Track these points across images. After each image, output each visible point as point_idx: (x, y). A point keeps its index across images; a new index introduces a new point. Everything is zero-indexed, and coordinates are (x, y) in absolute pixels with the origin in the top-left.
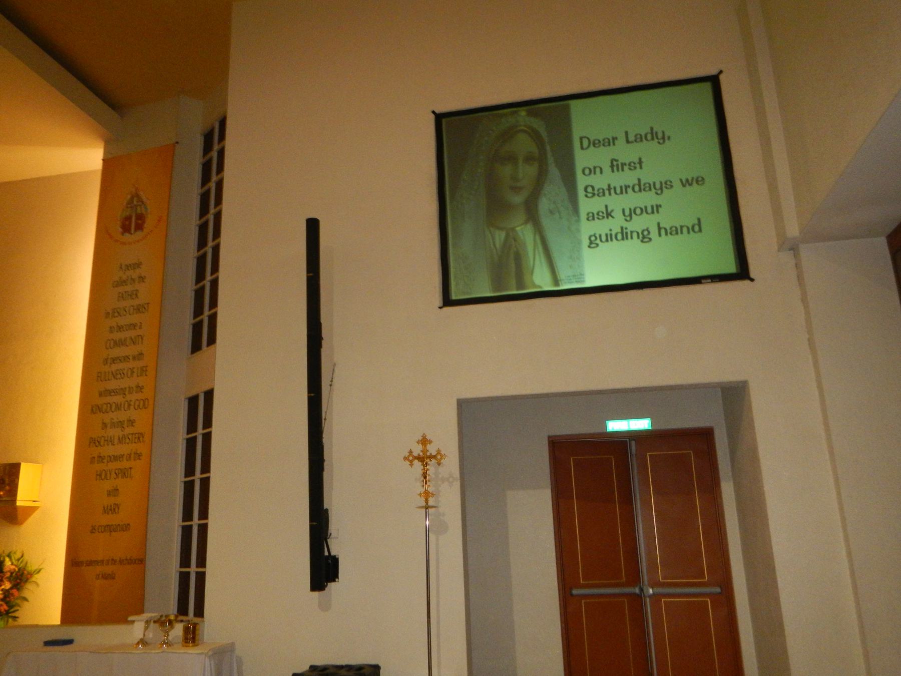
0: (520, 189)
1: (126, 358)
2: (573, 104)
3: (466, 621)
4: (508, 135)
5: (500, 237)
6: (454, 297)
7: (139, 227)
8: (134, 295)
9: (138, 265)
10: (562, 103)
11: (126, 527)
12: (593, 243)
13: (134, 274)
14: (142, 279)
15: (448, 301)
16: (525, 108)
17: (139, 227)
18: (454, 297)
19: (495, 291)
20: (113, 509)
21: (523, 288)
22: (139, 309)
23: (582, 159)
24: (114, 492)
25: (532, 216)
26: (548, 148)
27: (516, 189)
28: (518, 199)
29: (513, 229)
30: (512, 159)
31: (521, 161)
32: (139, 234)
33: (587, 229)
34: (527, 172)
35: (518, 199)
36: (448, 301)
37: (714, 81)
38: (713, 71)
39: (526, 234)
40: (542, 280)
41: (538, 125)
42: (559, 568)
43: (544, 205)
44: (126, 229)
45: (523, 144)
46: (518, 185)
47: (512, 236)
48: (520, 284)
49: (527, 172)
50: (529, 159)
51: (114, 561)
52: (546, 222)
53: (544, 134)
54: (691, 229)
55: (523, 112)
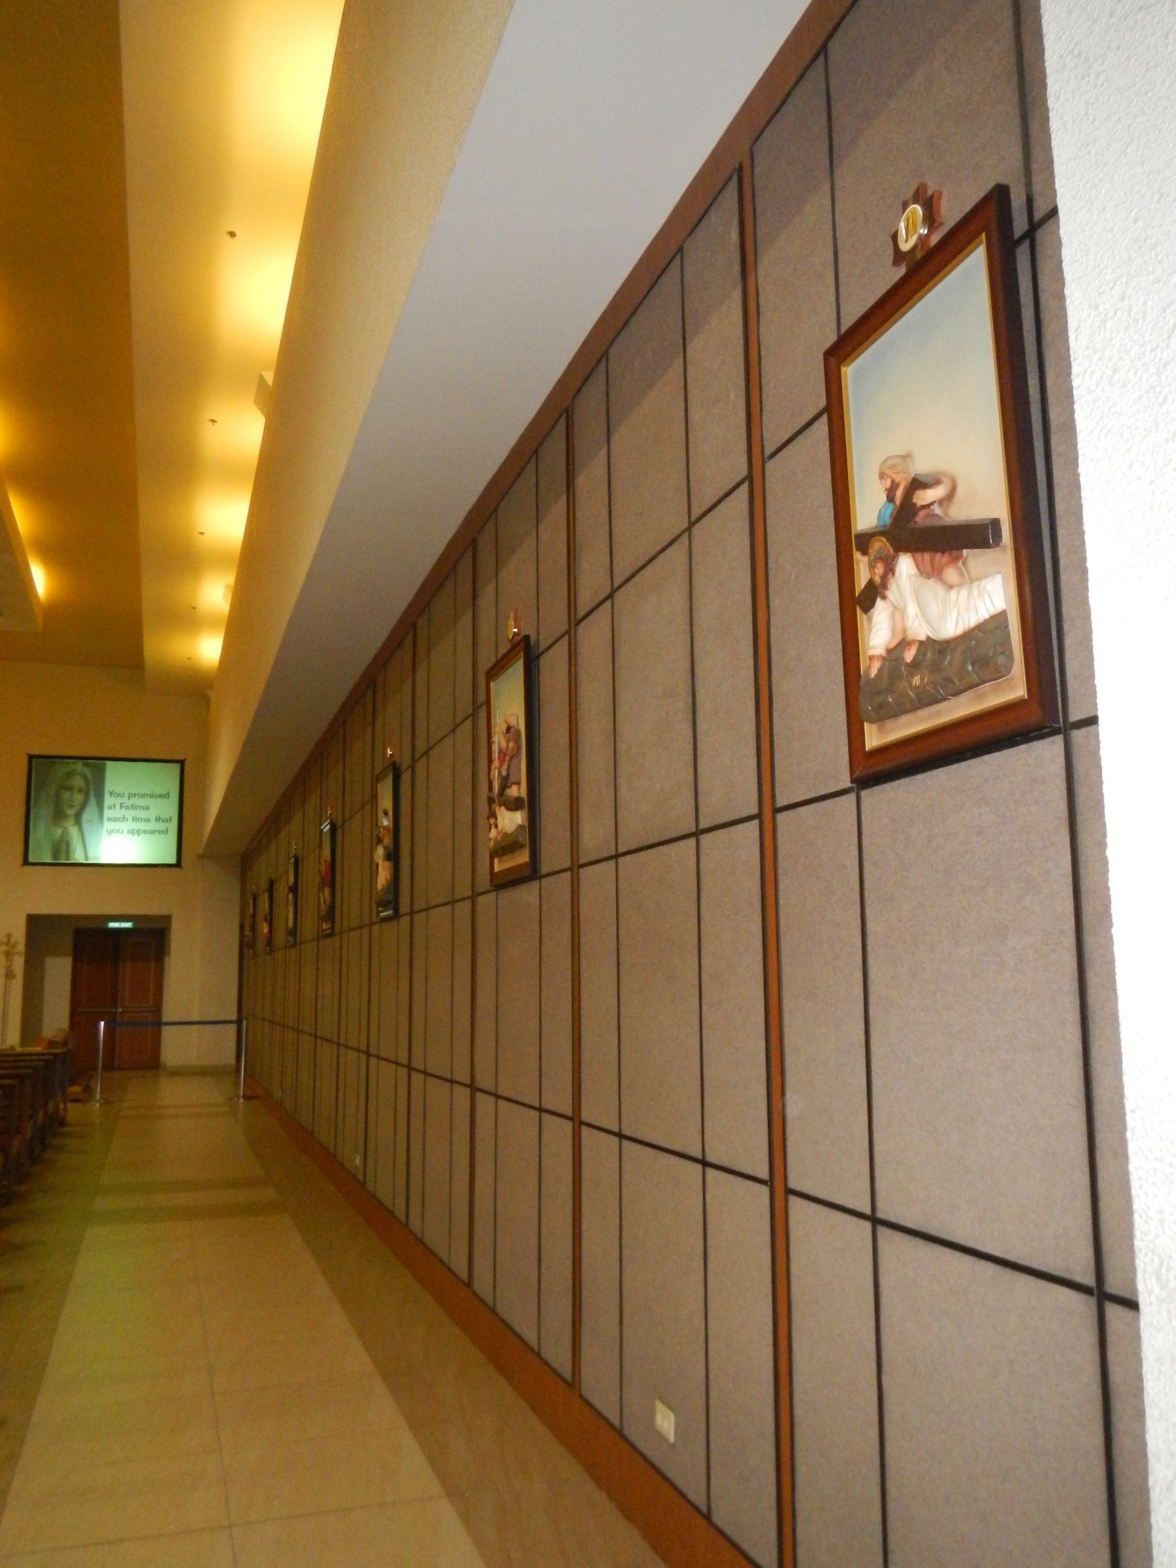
0: (73, 806)
2: (109, 764)
3: (1081, 505)
4: (69, 775)
5: (59, 831)
6: (31, 860)
10: (101, 762)
12: (111, 832)
15: (26, 862)
16: (81, 761)
18: (31, 860)
19: (54, 859)
21: (68, 860)
23: (108, 800)
25: (78, 821)
26: (91, 786)
27: (71, 806)
28: (71, 812)
29: (67, 828)
30: (70, 789)
31: (75, 791)
33: (108, 825)
34: (78, 798)
35: (71, 812)
36: (26, 862)
37: (182, 763)
38: (182, 758)
39: (73, 831)
40: (78, 857)
41: (87, 771)
42: (374, 881)
43: (85, 817)
45: (78, 782)
46: (73, 804)
47: (65, 833)
48: (68, 857)
49: (78, 798)
50: (80, 791)
52: (85, 826)
53: (90, 777)
54: (163, 832)
55: (80, 763)
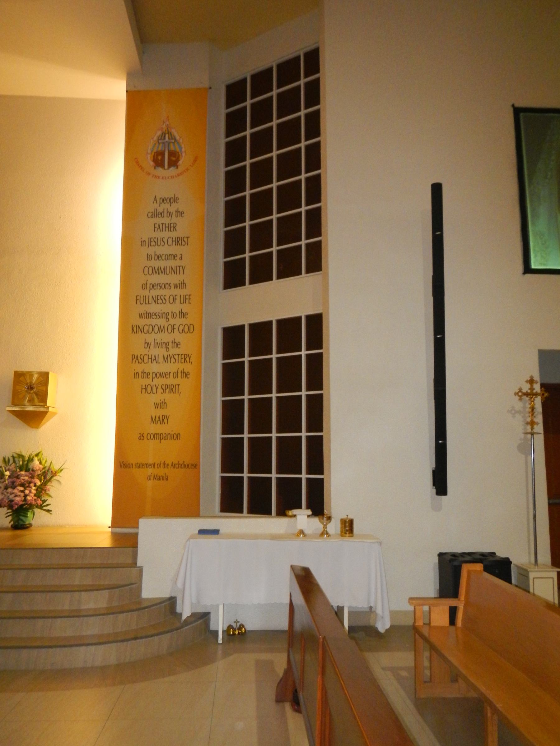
1: (167, 286)
7: (174, 163)
8: (172, 227)
9: (174, 200)
11: (177, 436)
13: (173, 208)
14: (180, 213)
17: (174, 163)
20: (163, 420)
22: (178, 241)
24: (163, 405)
32: (173, 171)
44: (158, 162)
51: (166, 465)
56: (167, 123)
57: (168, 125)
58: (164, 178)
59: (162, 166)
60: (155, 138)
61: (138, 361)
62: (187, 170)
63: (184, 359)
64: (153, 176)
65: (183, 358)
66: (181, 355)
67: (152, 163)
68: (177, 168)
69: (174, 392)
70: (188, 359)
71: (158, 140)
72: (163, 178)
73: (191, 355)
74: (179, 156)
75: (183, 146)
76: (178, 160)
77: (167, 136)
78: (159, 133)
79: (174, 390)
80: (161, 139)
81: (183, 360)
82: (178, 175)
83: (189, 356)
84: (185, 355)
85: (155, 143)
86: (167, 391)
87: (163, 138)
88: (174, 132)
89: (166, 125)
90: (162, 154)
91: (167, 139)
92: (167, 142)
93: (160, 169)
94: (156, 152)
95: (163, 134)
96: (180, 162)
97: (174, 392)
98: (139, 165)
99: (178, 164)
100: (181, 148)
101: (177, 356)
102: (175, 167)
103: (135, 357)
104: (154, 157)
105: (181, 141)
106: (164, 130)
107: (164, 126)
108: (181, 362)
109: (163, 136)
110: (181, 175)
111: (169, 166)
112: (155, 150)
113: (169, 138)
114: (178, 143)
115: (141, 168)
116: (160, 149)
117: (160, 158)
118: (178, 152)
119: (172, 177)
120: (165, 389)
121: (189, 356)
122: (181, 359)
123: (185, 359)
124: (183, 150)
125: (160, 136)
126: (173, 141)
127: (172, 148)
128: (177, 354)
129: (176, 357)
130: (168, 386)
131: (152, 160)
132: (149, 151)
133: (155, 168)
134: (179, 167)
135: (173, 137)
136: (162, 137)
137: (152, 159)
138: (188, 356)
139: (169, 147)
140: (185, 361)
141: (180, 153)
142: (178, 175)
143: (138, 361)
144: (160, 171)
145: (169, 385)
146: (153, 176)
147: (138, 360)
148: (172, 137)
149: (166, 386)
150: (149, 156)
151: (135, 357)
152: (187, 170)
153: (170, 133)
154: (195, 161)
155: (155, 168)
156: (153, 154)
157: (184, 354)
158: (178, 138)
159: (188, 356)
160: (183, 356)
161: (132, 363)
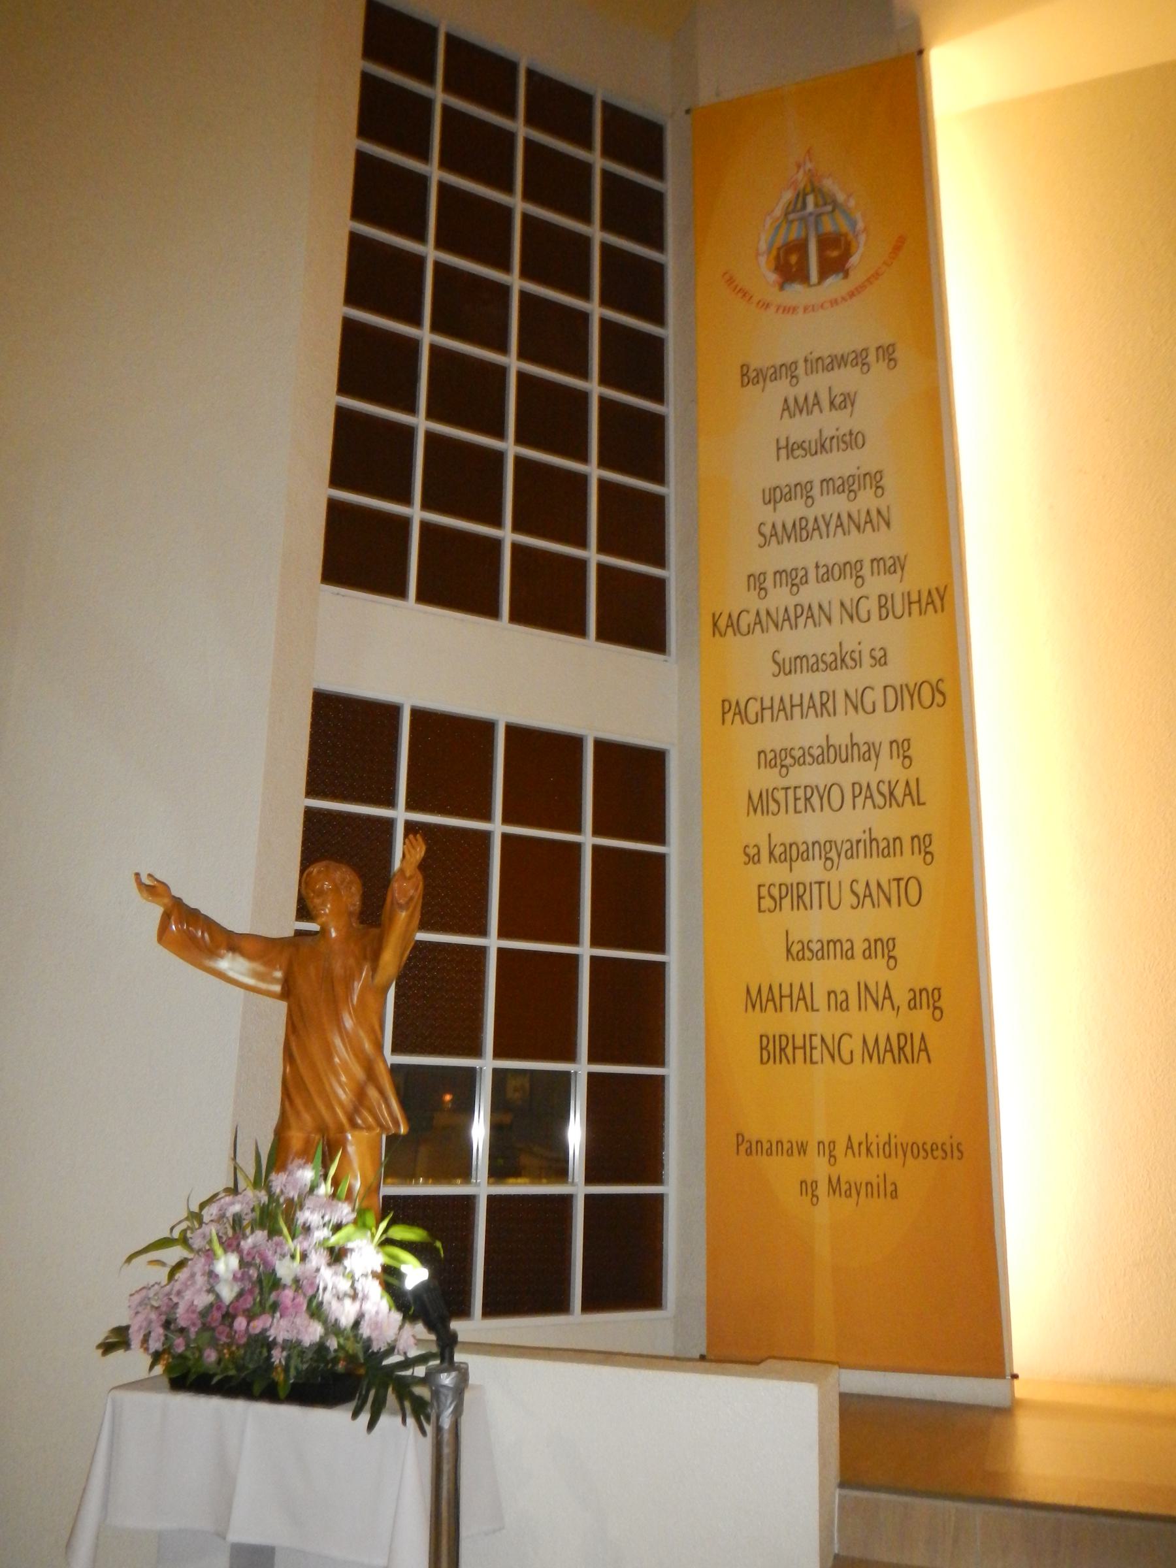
32: (835, 285)
56: (809, 166)
57: (810, 170)
58: (810, 308)
59: (804, 278)
60: (778, 212)
61: (873, 801)
62: (877, 275)
63: (803, 800)
64: (778, 309)
65: (800, 799)
66: (796, 788)
67: (773, 277)
68: (846, 275)
69: (808, 904)
70: (815, 800)
71: (786, 214)
72: (805, 309)
73: (897, 782)
74: (848, 244)
75: (858, 216)
76: (847, 255)
77: (810, 200)
78: (788, 195)
79: (807, 898)
80: (793, 211)
81: (801, 804)
82: (852, 295)
83: (818, 791)
84: (806, 787)
85: (777, 224)
86: (786, 902)
87: (799, 205)
88: (828, 184)
89: (805, 172)
90: (800, 247)
91: (810, 207)
92: (811, 214)
93: (797, 288)
94: (782, 247)
95: (798, 195)
96: (854, 260)
97: (808, 904)
98: (738, 289)
99: (847, 266)
100: (853, 224)
101: (784, 791)
102: (841, 275)
103: (861, 789)
104: (778, 257)
105: (852, 203)
106: (802, 186)
107: (800, 175)
108: (796, 812)
109: (800, 199)
110: (859, 292)
111: (823, 275)
112: (779, 242)
113: (816, 205)
114: (846, 213)
115: (745, 294)
116: (793, 235)
117: (794, 259)
118: (846, 235)
119: (834, 303)
120: (781, 898)
121: (818, 791)
122: (796, 799)
123: (807, 800)
124: (860, 225)
125: (790, 203)
126: (829, 208)
127: (828, 226)
128: (782, 789)
129: (780, 796)
130: (789, 888)
131: (773, 267)
132: (763, 246)
133: (782, 288)
134: (851, 273)
135: (829, 201)
136: (796, 203)
137: (773, 265)
138: (815, 791)
139: (817, 228)
140: (808, 805)
141: (851, 236)
142: (852, 295)
143: (873, 801)
144: (796, 293)
145: (792, 885)
146: (778, 309)
147: (871, 797)
148: (828, 201)
149: (784, 889)
150: (763, 260)
151: (861, 789)
152: (877, 275)
153: (816, 190)
154: (897, 249)
155: (782, 288)
156: (774, 252)
157: (804, 783)
158: (841, 197)
159: (815, 791)
160: (800, 792)
161: (854, 807)
